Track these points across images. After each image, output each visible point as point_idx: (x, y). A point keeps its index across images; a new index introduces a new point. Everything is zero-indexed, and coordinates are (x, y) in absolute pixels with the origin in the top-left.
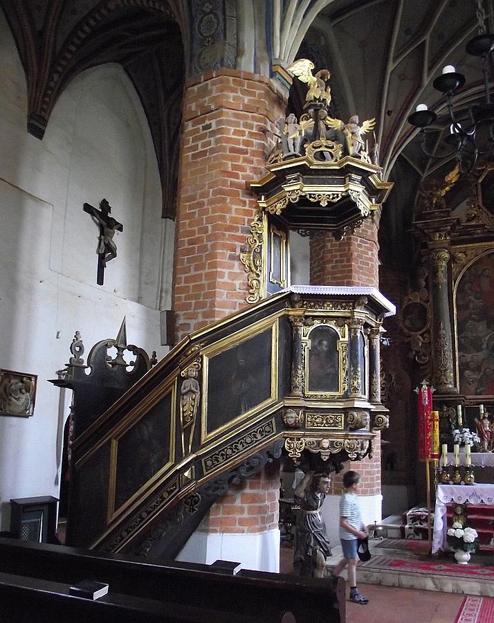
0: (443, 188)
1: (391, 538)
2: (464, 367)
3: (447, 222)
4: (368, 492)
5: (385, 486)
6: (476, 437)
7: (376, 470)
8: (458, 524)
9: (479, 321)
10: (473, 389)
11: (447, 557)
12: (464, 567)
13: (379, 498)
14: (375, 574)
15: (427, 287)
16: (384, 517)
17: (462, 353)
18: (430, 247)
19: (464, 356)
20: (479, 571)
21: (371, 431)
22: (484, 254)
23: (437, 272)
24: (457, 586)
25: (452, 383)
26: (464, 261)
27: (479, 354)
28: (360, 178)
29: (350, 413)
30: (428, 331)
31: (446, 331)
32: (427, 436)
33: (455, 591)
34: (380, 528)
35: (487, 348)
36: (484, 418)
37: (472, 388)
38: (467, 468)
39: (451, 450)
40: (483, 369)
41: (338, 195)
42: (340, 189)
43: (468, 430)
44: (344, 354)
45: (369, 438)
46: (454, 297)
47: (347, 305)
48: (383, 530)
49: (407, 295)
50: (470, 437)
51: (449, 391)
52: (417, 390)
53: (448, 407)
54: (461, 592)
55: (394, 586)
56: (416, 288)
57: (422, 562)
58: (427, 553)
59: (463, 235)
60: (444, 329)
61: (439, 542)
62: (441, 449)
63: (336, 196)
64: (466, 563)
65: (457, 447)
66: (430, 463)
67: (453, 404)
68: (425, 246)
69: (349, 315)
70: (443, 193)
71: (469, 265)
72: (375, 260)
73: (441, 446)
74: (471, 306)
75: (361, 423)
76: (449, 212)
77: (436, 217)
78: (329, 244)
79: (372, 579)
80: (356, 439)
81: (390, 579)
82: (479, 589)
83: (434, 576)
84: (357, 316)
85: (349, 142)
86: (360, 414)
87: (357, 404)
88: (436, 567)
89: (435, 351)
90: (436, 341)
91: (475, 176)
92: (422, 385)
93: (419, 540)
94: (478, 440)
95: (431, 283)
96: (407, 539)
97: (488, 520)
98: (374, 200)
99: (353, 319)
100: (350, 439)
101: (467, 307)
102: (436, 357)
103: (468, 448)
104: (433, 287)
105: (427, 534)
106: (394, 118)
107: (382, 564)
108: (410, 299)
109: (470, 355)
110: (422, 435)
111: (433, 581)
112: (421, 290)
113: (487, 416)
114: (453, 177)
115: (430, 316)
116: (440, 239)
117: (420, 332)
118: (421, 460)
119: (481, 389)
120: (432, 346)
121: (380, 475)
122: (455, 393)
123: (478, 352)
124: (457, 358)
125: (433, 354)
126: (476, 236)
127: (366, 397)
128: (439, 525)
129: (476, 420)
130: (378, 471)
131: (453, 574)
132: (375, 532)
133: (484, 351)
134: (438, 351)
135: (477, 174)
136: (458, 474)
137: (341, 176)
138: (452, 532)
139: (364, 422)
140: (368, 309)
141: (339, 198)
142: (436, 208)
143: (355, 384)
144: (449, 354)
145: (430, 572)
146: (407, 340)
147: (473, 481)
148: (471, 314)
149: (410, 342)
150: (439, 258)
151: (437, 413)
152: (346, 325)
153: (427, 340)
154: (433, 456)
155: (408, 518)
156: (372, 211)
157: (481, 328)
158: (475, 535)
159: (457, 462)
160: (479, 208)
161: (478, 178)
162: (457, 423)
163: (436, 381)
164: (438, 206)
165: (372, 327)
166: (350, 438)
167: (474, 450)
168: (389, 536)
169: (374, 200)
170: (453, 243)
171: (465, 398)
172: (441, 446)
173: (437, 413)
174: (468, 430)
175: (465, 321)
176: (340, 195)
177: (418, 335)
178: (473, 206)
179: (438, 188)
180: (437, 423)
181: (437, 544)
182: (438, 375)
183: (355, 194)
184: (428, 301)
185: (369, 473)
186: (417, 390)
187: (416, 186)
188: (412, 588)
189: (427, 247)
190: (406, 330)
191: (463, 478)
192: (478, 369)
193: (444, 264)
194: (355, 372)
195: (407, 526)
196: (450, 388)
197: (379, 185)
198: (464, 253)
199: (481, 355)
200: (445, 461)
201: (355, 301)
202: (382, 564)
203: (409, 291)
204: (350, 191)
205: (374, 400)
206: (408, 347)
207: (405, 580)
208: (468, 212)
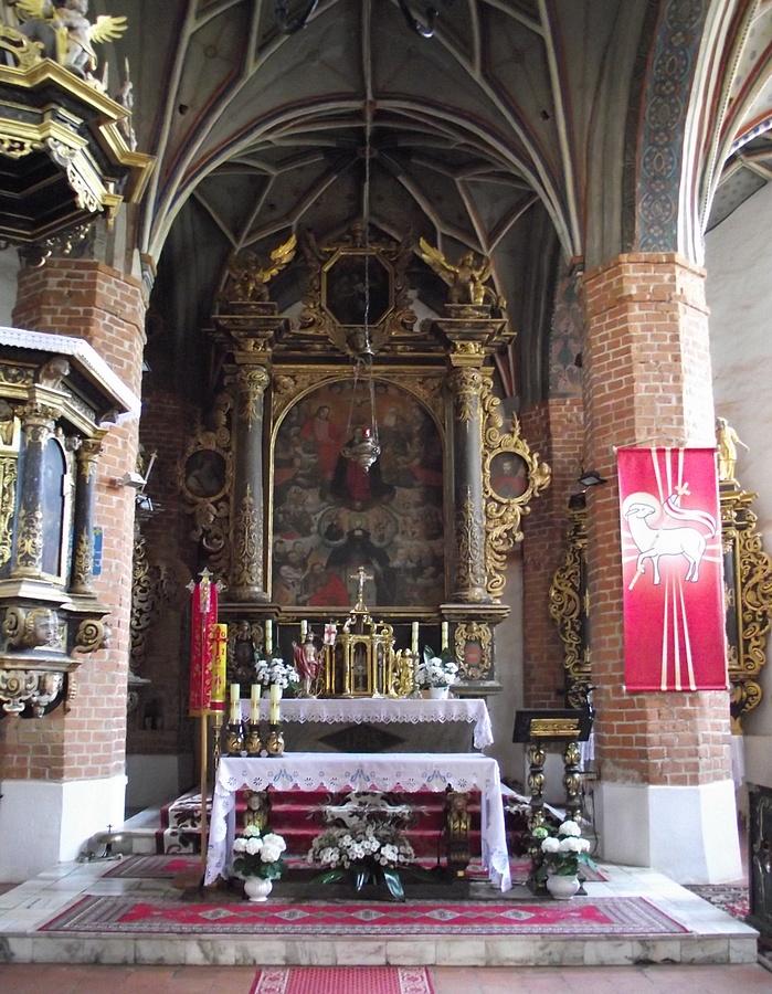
0: (267, 269)
1: (138, 854)
2: (281, 559)
3: (268, 323)
4: (98, 771)
5: (138, 758)
6: (293, 673)
7: (116, 730)
8: (253, 829)
9: (308, 487)
10: (292, 597)
11: (231, 888)
12: (259, 908)
13: (121, 781)
14: (88, 944)
15: (228, 425)
16: (130, 811)
17: (278, 538)
18: (238, 361)
19: (281, 542)
20: (284, 915)
21: (69, 653)
22: (323, 383)
23: (247, 401)
24: (244, 950)
25: (258, 585)
26: (291, 390)
27: (304, 540)
28: (78, 121)
29: (9, 611)
30: (226, 499)
31: (254, 497)
32: (206, 669)
33: (241, 962)
34: (118, 838)
35: (319, 531)
36: (307, 641)
37: (292, 594)
38: (273, 728)
39: (246, 694)
40: (310, 564)
41: (22, 144)
42: (29, 134)
43: (280, 661)
44: (7, 480)
45: (64, 669)
46: (272, 446)
47: (20, 374)
48: (123, 841)
49: (194, 436)
50: (283, 673)
51: (254, 596)
52: (191, 586)
53: (251, 624)
54: (250, 962)
55: (125, 964)
56: (211, 426)
57: (185, 904)
58: (198, 883)
59: (292, 350)
60: (251, 495)
61: (218, 865)
62: (228, 694)
63: (17, 145)
64: (264, 899)
65: (256, 689)
66: (209, 717)
67: (258, 618)
68: (231, 359)
69: (25, 395)
70: (267, 278)
71: (298, 398)
72: (135, 359)
73: (228, 688)
74: (297, 462)
75: (35, 634)
76: (273, 308)
77: (251, 313)
78: (49, 318)
79: (80, 954)
80: (26, 671)
81: (118, 949)
82: (284, 953)
83: (204, 936)
84: (41, 399)
85: (62, 44)
86: (34, 612)
87: (26, 591)
88: (208, 914)
89: (235, 533)
90: (237, 514)
91: (320, 260)
92: (202, 577)
93: (189, 854)
94: (295, 677)
95: (235, 419)
96: (167, 854)
97: (306, 812)
98: (112, 186)
99: (32, 404)
100: (8, 670)
101: (290, 463)
102: (236, 540)
103: (277, 692)
104: (239, 425)
105: (198, 842)
106: (192, 120)
107: (105, 918)
108: (199, 444)
109: (292, 542)
110: (197, 667)
111: (200, 946)
112: (218, 431)
113: (311, 639)
114: (284, 252)
115: (230, 473)
116: (256, 349)
117: (212, 499)
118: (193, 713)
119: (306, 596)
120: (231, 523)
121: (124, 740)
122: (264, 601)
123: (304, 536)
124: (270, 546)
125: (231, 534)
126: (313, 353)
127: (63, 580)
128: (219, 831)
129: (295, 645)
130: (119, 734)
131: (238, 927)
132: (109, 847)
133: (313, 537)
134: (241, 532)
135: (321, 257)
136: (259, 737)
137: (34, 106)
138: (240, 844)
139: (42, 632)
140: (67, 388)
141: (25, 152)
142: (253, 298)
143: (28, 547)
144: (258, 537)
145: (196, 927)
146: (189, 511)
147: (281, 748)
148: (296, 475)
149: (194, 513)
150: (252, 380)
151: (224, 627)
152: (17, 420)
153: (222, 513)
154: (215, 706)
155: (171, 815)
156: (107, 207)
157: (310, 500)
158: (281, 847)
159: (256, 717)
160: (322, 310)
161: (323, 263)
162: (264, 650)
163: (231, 568)
164: (257, 296)
165: (84, 436)
166: (8, 666)
167: (287, 694)
168: (135, 851)
169: (112, 186)
170: (276, 360)
171: (279, 609)
172: (228, 688)
173: (224, 627)
174: (280, 661)
175: (288, 485)
176: (27, 146)
177: (209, 503)
178: (312, 306)
179: (258, 267)
180: (223, 646)
181: (214, 868)
182: (236, 571)
183: (61, 150)
184: (227, 449)
185: (101, 737)
186: (191, 586)
187: (224, 261)
188: (160, 964)
189: (234, 362)
190: (189, 495)
191: (265, 744)
192: (303, 564)
193: (260, 390)
194: (30, 521)
195: (168, 831)
196: (256, 593)
197: (124, 155)
198: (293, 377)
199: (308, 542)
200: (237, 715)
201: (40, 368)
202: (105, 918)
203: (199, 429)
204: (51, 140)
205: (82, 588)
206: (190, 521)
207: (148, 950)
208: (303, 314)
